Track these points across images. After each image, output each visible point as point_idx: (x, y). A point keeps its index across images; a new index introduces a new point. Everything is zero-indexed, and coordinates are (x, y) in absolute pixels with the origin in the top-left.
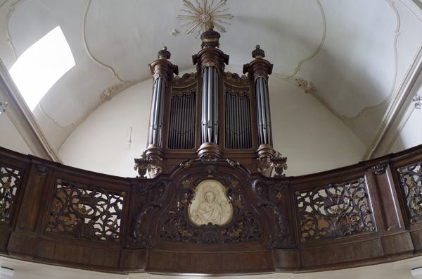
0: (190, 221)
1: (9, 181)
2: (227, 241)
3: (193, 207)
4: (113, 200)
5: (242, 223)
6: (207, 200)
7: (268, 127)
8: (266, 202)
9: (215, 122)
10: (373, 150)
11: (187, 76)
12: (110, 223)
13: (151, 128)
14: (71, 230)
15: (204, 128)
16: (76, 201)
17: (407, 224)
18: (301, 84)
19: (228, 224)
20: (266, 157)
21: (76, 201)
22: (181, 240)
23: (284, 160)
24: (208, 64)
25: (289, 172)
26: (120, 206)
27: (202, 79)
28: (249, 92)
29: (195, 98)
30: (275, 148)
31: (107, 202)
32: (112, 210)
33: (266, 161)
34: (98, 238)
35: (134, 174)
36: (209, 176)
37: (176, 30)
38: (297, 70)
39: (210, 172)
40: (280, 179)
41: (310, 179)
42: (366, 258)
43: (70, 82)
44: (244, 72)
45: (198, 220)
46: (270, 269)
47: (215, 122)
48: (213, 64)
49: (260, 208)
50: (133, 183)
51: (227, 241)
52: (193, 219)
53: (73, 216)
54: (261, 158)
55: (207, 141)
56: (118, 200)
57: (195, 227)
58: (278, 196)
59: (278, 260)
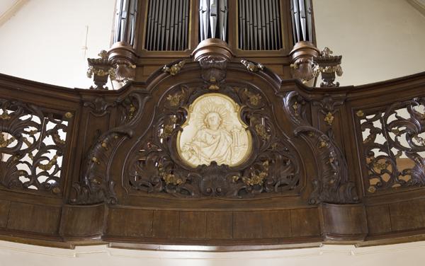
0: (179, 158)
2: (243, 191)
3: (185, 138)
5: (267, 163)
6: (208, 126)
7: (309, 16)
8: (308, 127)
12: (45, 162)
15: (203, 17)
22: (164, 191)
23: (337, 60)
26: (63, 135)
33: (305, 69)
34: (25, 186)
35: (88, 83)
36: (212, 87)
40: (331, 91)
47: (222, 8)
49: (297, 137)
50: (85, 97)
51: (243, 191)
52: (185, 156)
54: (298, 64)
55: (209, 36)
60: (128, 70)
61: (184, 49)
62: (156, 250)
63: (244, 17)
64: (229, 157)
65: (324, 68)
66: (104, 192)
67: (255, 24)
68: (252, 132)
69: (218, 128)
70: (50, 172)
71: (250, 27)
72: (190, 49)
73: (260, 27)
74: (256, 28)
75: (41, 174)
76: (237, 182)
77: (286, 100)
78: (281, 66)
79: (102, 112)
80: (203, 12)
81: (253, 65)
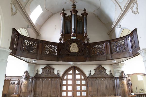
0: (70, 51)
1: (35, 45)
3: (71, 49)
6: (73, 47)
8: (85, 48)
9: (75, 28)
10: (109, 32)
11: (69, 16)
14: (48, 54)
15: (72, 29)
16: (48, 48)
17: (111, 54)
18: (95, 14)
21: (48, 48)
23: (89, 39)
24: (73, 14)
25: (90, 42)
26: (57, 48)
27: (72, 17)
29: (71, 21)
30: (87, 34)
31: (54, 48)
33: (85, 37)
35: (59, 42)
38: (94, 11)
40: (88, 43)
43: (42, 16)
44: (81, 15)
46: (86, 61)
51: (77, 55)
53: (48, 51)
56: (56, 47)
59: (87, 59)
62: (21, 59)
71: (78, 30)
77: (83, 44)
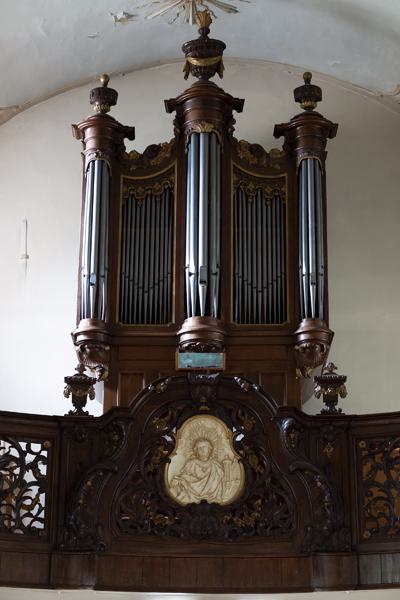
0: (168, 496)
2: (233, 534)
3: (173, 469)
4: (30, 458)
5: (260, 501)
6: (197, 456)
7: (321, 279)
11: (153, 150)
12: (28, 502)
13: (84, 280)
15: (190, 281)
19: (235, 501)
20: (313, 348)
22: (152, 532)
23: (343, 380)
24: (199, 129)
26: (43, 469)
28: (285, 189)
32: (29, 477)
34: (10, 530)
35: (63, 406)
36: (203, 408)
37: (124, 13)
39: (203, 400)
41: (387, 421)
42: (375, 582)
45: (183, 494)
46: (310, 589)
47: (214, 269)
48: (209, 128)
49: (292, 473)
50: (64, 424)
51: (233, 534)
52: (173, 492)
54: (304, 348)
55: (198, 313)
57: (176, 508)
58: (326, 450)
60: (101, 355)
61: (167, 322)
63: (240, 274)
64: (220, 493)
65: (326, 389)
66: (92, 538)
67: (255, 285)
68: (244, 465)
69: (208, 458)
70: (34, 512)
72: (174, 322)
73: (260, 289)
74: (255, 291)
75: (25, 515)
76: (228, 522)
78: (284, 347)
79: (83, 440)
80: (190, 274)
81: (248, 384)
